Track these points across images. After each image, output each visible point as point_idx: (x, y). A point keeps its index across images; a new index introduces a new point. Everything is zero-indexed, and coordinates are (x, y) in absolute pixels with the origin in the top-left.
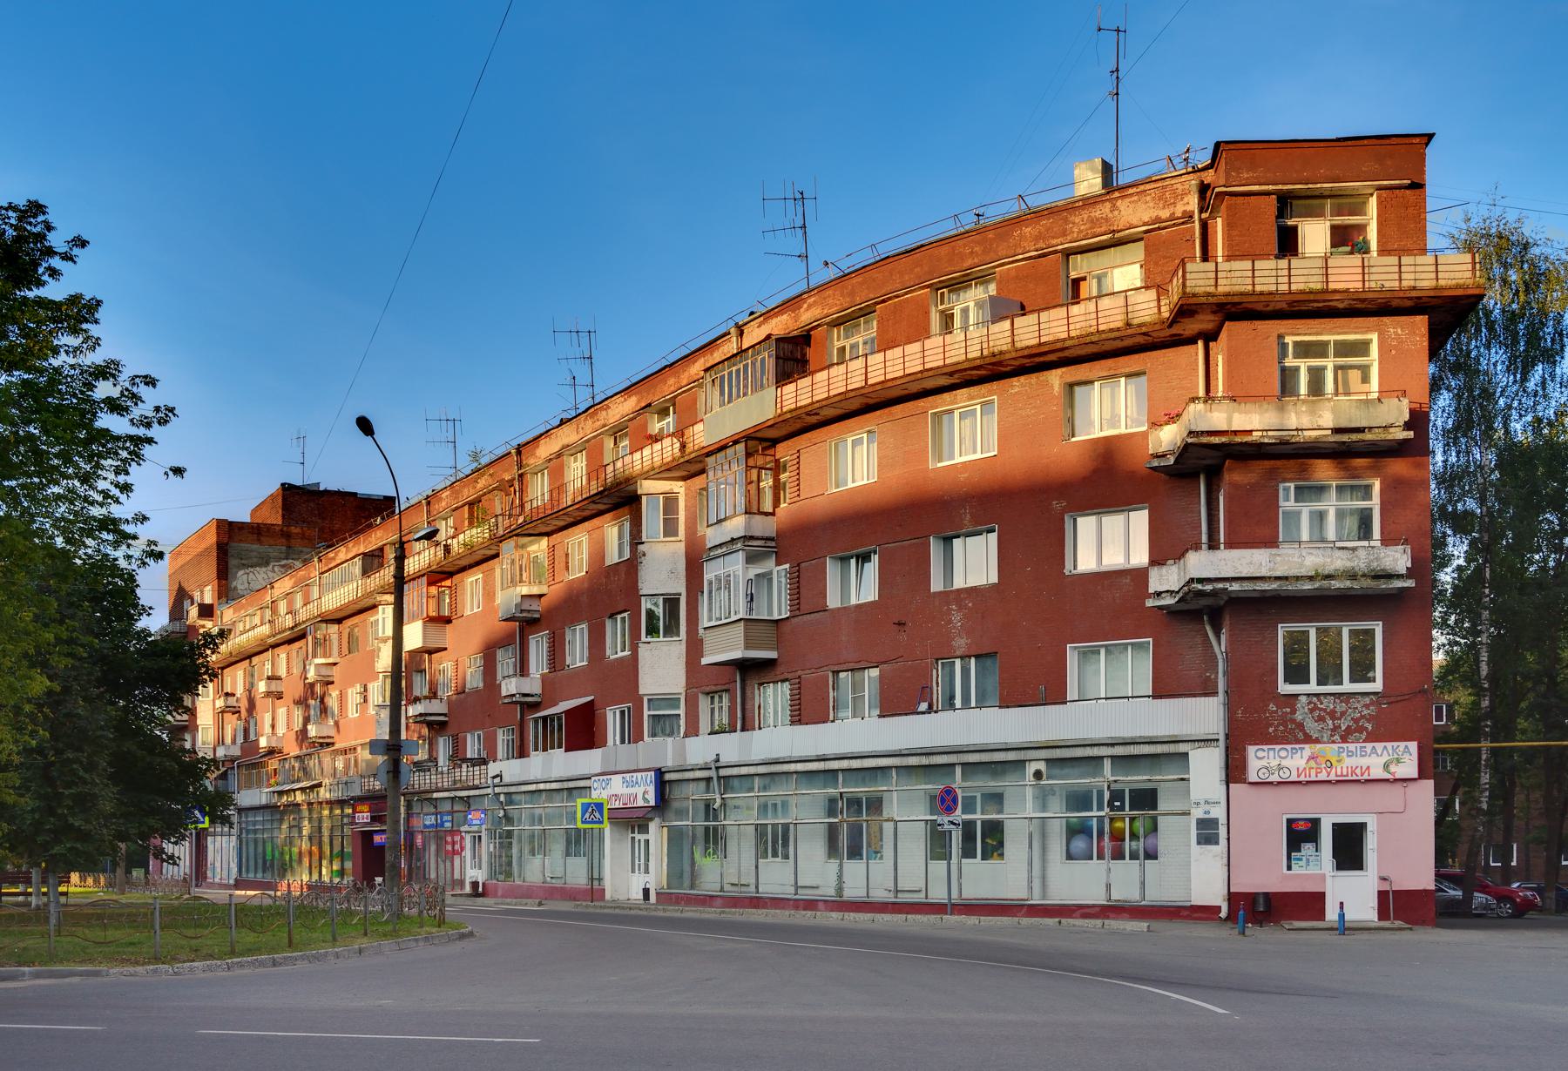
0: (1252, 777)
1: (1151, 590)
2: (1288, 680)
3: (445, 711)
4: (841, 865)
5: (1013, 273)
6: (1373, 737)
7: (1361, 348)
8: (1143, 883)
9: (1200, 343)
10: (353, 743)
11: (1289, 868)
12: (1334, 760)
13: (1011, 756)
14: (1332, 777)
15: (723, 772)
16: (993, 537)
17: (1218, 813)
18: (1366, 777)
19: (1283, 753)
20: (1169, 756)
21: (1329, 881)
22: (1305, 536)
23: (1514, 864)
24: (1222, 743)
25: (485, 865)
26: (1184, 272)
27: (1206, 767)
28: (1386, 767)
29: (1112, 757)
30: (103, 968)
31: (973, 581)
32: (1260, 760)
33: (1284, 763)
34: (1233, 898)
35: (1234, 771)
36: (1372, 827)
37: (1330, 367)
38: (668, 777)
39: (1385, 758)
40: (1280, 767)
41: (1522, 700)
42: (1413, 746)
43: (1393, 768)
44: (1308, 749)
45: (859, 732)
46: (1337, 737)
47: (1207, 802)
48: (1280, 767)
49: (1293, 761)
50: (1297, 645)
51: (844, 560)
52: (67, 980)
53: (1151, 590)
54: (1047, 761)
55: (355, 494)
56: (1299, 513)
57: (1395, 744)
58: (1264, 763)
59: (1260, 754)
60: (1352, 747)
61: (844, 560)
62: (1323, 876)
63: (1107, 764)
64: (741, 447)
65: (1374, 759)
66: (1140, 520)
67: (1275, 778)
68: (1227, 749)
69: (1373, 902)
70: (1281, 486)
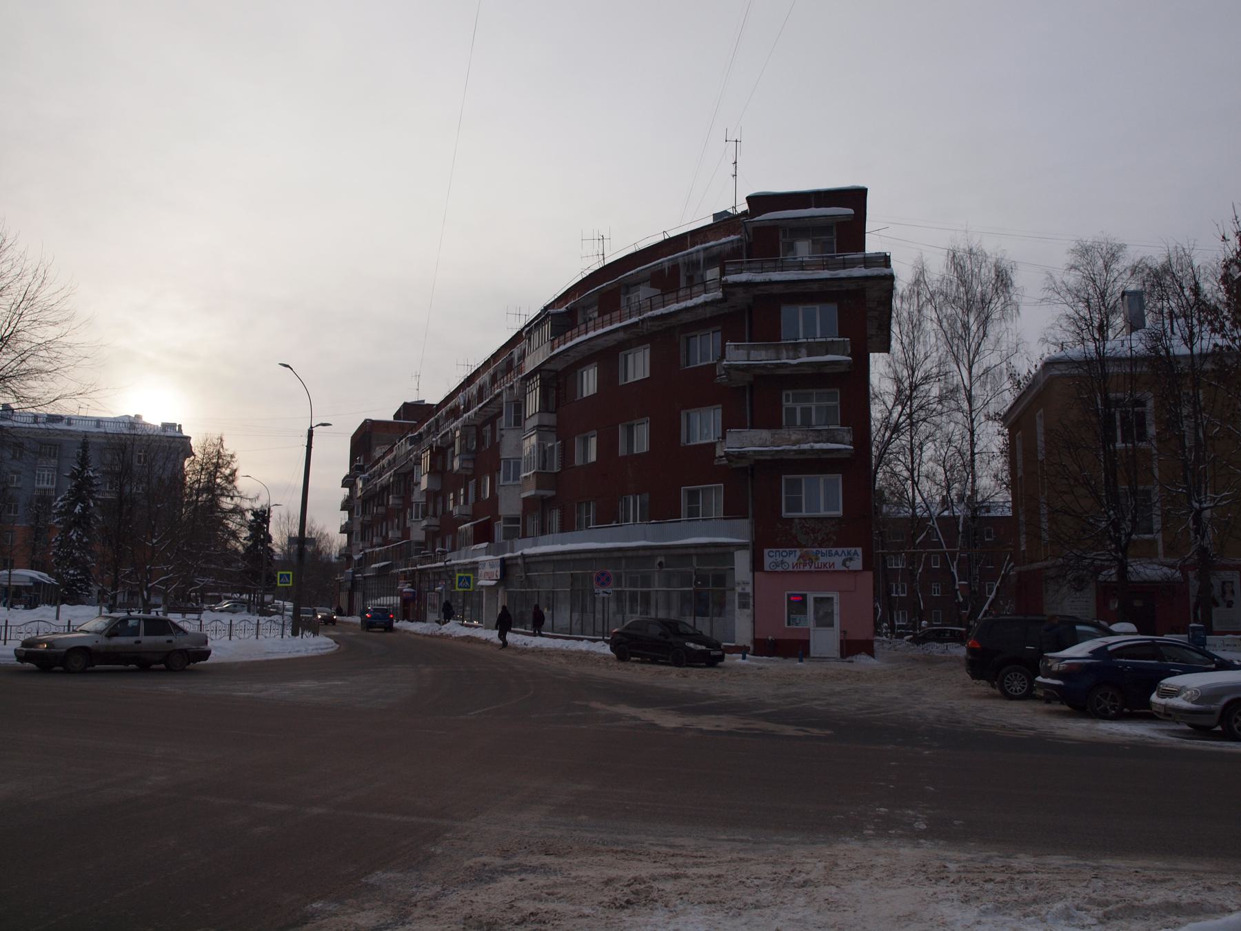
0: (767, 568)
5: (729, 247)
6: (837, 545)
9: (844, 446)
13: (648, 553)
16: (648, 352)
17: (749, 589)
20: (724, 553)
23: (456, 464)
27: (742, 561)
28: (844, 564)
32: (771, 558)
34: (756, 642)
35: (757, 564)
38: (508, 562)
40: (782, 562)
42: (859, 550)
45: (632, 536)
48: (782, 562)
49: (791, 559)
51: (303, 542)
52: (649, 715)
55: (413, 412)
60: (824, 550)
61: (303, 542)
63: (695, 559)
64: (547, 328)
65: (835, 558)
66: (874, 357)
67: (779, 569)
69: (837, 645)
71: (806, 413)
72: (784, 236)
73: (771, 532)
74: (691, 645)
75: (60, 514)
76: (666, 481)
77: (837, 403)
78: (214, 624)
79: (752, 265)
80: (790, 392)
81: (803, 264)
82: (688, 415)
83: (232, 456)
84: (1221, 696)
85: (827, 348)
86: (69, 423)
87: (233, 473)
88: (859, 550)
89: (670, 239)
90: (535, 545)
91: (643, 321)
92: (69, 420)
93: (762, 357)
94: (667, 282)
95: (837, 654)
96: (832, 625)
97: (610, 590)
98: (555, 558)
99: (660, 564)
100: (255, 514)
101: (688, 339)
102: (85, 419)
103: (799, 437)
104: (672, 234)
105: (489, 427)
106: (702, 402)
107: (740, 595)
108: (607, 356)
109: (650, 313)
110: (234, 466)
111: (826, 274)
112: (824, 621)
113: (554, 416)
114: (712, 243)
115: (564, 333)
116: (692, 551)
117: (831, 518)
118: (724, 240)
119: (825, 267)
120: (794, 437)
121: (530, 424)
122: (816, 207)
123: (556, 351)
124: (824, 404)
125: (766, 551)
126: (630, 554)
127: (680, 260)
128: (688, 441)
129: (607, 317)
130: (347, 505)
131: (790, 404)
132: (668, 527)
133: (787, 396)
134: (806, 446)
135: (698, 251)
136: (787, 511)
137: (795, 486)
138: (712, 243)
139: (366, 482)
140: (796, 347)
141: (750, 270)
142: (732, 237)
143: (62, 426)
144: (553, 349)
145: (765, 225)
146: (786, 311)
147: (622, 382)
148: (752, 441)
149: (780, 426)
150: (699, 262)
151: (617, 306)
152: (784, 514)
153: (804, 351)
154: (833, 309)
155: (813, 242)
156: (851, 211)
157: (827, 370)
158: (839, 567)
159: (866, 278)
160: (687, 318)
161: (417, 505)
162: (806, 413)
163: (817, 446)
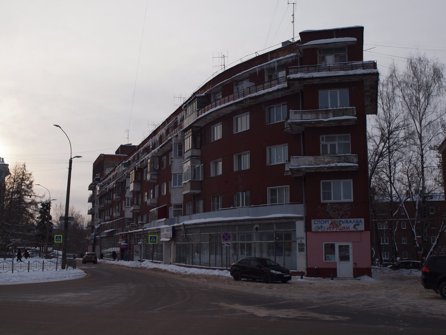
0: (313, 230)
1: (286, 170)
3: (139, 209)
5: (290, 60)
10: (306, 280)
11: (325, 260)
12: (338, 224)
13: (250, 223)
14: (338, 230)
15: (186, 227)
17: (304, 241)
18: (348, 230)
19: (322, 222)
20: (289, 223)
21: (338, 264)
22: (329, 152)
24: (304, 219)
27: (300, 226)
28: (354, 227)
29: (276, 223)
33: (323, 225)
34: (308, 269)
35: (308, 228)
36: (351, 247)
37: (337, 144)
39: (354, 224)
40: (322, 227)
41: (150, 162)
42: (363, 220)
43: (356, 227)
44: (330, 221)
46: (339, 217)
47: (301, 238)
48: (322, 227)
49: (326, 225)
53: (286, 170)
54: (259, 224)
56: (327, 145)
57: (357, 219)
59: (315, 222)
60: (344, 220)
62: (336, 263)
64: (195, 104)
65: (349, 224)
67: (320, 230)
68: (306, 221)
70: (321, 137)
71: (333, 147)
72: (320, 53)
74: (274, 271)
76: (260, 184)
77: (349, 141)
79: (303, 69)
80: (324, 136)
81: (330, 68)
82: (270, 149)
83: (30, 174)
85: (343, 112)
88: (363, 220)
91: (245, 100)
93: (309, 117)
94: (258, 79)
95: (352, 276)
97: (230, 243)
98: (201, 226)
99: (257, 229)
101: (269, 109)
104: (260, 53)
105: (165, 157)
107: (299, 244)
108: (227, 119)
110: (31, 179)
111: (342, 73)
112: (345, 258)
113: (199, 150)
116: (274, 221)
118: (288, 56)
119: (342, 69)
120: (327, 160)
121: (187, 155)
123: (200, 117)
125: (313, 221)
127: (265, 67)
128: (270, 163)
130: (91, 199)
131: (324, 142)
132: (260, 209)
133: (323, 138)
134: (333, 165)
135: (274, 62)
136: (324, 199)
137: (328, 186)
139: (101, 187)
140: (327, 112)
141: (302, 71)
142: (292, 55)
144: (198, 116)
146: (321, 93)
147: (235, 132)
148: (304, 163)
149: (319, 154)
150: (274, 68)
152: (322, 201)
153: (331, 114)
154: (346, 92)
156: (355, 39)
157: (344, 124)
158: (352, 229)
159: (364, 75)
162: (333, 147)
163: (339, 164)
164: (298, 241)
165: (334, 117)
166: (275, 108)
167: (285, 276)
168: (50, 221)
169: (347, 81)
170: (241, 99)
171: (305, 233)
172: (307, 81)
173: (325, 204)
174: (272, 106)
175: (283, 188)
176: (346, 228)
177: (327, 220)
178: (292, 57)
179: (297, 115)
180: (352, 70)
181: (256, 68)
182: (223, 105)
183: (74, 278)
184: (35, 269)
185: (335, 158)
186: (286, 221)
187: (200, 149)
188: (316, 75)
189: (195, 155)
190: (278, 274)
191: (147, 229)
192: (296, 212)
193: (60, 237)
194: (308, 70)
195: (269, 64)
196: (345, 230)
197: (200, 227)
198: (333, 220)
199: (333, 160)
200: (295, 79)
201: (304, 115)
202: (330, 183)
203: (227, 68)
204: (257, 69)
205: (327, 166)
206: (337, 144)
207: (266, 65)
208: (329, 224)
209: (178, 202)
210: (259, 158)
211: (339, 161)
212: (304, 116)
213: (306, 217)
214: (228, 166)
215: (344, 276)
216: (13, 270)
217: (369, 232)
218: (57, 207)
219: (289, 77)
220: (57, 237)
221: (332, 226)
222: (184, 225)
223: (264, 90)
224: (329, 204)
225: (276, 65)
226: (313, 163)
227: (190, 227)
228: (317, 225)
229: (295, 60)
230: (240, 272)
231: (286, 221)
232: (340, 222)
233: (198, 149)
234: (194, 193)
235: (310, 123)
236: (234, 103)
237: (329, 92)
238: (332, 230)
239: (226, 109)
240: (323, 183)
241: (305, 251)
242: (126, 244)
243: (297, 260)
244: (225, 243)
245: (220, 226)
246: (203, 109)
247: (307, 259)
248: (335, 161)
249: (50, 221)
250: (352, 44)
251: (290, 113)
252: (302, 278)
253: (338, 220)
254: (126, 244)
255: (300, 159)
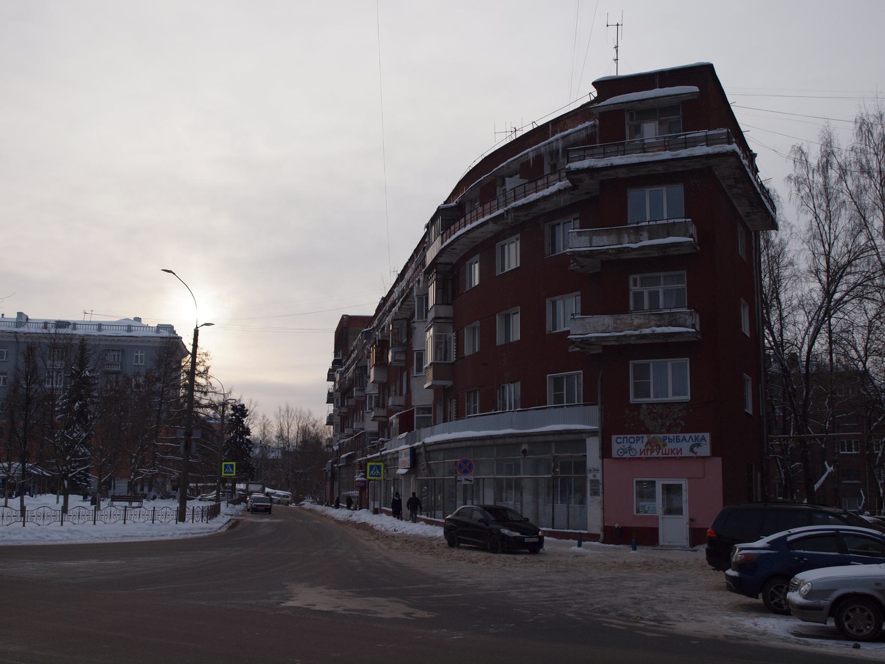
0: (614, 454)
2: (636, 396)
4: (22, 501)
5: (583, 134)
7: (864, 611)
8: (553, 519)
12: (661, 444)
13: (514, 441)
14: (660, 455)
15: (428, 449)
17: (599, 476)
18: (679, 455)
19: (632, 440)
20: (576, 440)
21: (660, 520)
22: (646, 306)
24: (600, 434)
25: (658, 274)
26: (779, 303)
27: (593, 446)
28: (692, 450)
30: (403, 616)
31: (515, 339)
32: (618, 444)
33: (633, 446)
34: (605, 529)
35: (606, 451)
36: (685, 487)
37: (661, 291)
39: (691, 443)
40: (630, 449)
42: (707, 436)
43: (695, 449)
46: (664, 430)
47: (595, 470)
48: (630, 449)
49: (639, 445)
50: (141, 362)
54: (529, 443)
56: (642, 293)
57: (697, 434)
58: (621, 446)
59: (619, 440)
60: (671, 436)
62: (657, 518)
65: (682, 444)
67: (627, 455)
71: (654, 296)
72: (631, 119)
73: (619, 419)
74: (506, 531)
75: (61, 411)
76: (539, 366)
77: (684, 285)
78: (41, 510)
79: (596, 151)
80: (638, 276)
81: (650, 146)
82: (554, 304)
83: (206, 355)
84: (833, 590)
85: (669, 229)
86: (75, 328)
87: (207, 369)
88: (707, 436)
89: (539, 127)
90: (432, 434)
91: (507, 211)
92: (75, 325)
93: (604, 242)
94: (532, 172)
95: (686, 543)
96: (681, 514)
97: (472, 478)
98: (443, 446)
99: (524, 452)
100: (234, 408)
101: (553, 228)
102: (90, 324)
103: (642, 321)
104: (540, 123)
106: (564, 290)
107: (592, 481)
108: (486, 248)
109: (513, 204)
110: (207, 364)
111: (667, 155)
112: (672, 510)
113: (450, 307)
114: (570, 131)
115: (450, 228)
116: (550, 438)
117: (680, 403)
118: (580, 127)
119: (666, 148)
120: (637, 322)
121: (431, 315)
122: (660, 87)
123: (445, 244)
124: (670, 286)
125: (614, 437)
126: (500, 441)
127: (543, 149)
128: (554, 328)
129: (487, 206)
130: (330, 398)
131: (638, 288)
132: (533, 414)
133: (635, 281)
134: (647, 331)
135: (557, 140)
136: (636, 396)
137: (642, 372)
138: (570, 131)
139: (342, 374)
140: (638, 230)
141: (592, 156)
142: (587, 124)
143: (69, 331)
144: (442, 244)
145: (617, 107)
146: (633, 194)
147: (498, 272)
148: (599, 328)
149: (626, 311)
150: (558, 151)
151: (493, 197)
152: (632, 400)
153: (645, 234)
154: (679, 190)
155: (660, 123)
156: (695, 89)
157: (673, 252)
158: (686, 453)
159: (708, 156)
160: (549, 207)
161: (371, 397)
162: (654, 296)
163: (659, 330)
164: (590, 476)
165: (650, 239)
166: (561, 225)
167: (526, 540)
168: (248, 437)
169: (681, 169)
170: (501, 211)
171: (600, 461)
172: (603, 173)
173: (639, 406)
174: (556, 222)
175: (574, 374)
176: (675, 451)
177: (640, 436)
178: (587, 128)
179: (583, 238)
180: (686, 148)
181: (529, 152)
182: (475, 223)
183: (182, 537)
184: (107, 521)
185: (652, 317)
186: (572, 437)
187: (452, 304)
188: (617, 160)
189: (442, 315)
190: (515, 537)
191: (387, 451)
192: (580, 420)
193: (232, 466)
194: (604, 153)
195: (549, 143)
196: (673, 455)
197: (443, 449)
198: (652, 436)
199: (649, 323)
200: (579, 171)
201: (594, 238)
202: (649, 364)
203: (744, 134)
204: (531, 154)
205: (636, 333)
206: (661, 291)
207: (545, 145)
208: (645, 443)
209: (425, 403)
210: (534, 321)
211: (659, 323)
212: (596, 240)
213: (603, 430)
214: (488, 336)
215: (671, 544)
216: (24, 522)
217: (720, 459)
218: (282, 413)
219: (570, 168)
220: (226, 466)
221: (649, 447)
222: (425, 445)
223: (536, 192)
224: (644, 406)
225: (561, 144)
226: (610, 329)
227: (435, 447)
228: (621, 446)
229: (592, 133)
230: (459, 534)
231: (572, 437)
232: (664, 440)
233: (448, 304)
234: (444, 386)
235: (606, 252)
236: (490, 219)
237: (647, 193)
238: (649, 456)
239: (481, 230)
240: (635, 366)
241: (601, 494)
242: (363, 479)
243: (589, 511)
244: (463, 478)
245: (469, 447)
246: (448, 231)
247: (603, 509)
248: (653, 323)
249: (248, 437)
250: (691, 98)
251: (605, 231)
252: (580, 545)
253: (662, 436)
254: (363, 479)
255: (587, 320)
